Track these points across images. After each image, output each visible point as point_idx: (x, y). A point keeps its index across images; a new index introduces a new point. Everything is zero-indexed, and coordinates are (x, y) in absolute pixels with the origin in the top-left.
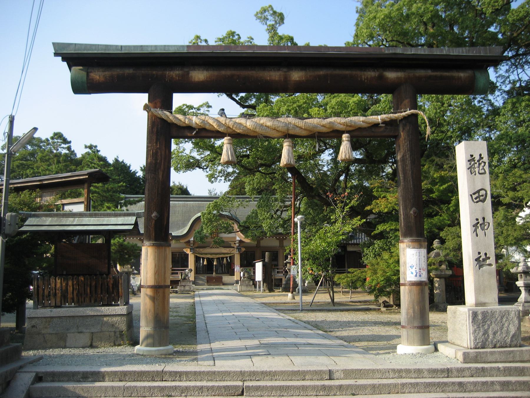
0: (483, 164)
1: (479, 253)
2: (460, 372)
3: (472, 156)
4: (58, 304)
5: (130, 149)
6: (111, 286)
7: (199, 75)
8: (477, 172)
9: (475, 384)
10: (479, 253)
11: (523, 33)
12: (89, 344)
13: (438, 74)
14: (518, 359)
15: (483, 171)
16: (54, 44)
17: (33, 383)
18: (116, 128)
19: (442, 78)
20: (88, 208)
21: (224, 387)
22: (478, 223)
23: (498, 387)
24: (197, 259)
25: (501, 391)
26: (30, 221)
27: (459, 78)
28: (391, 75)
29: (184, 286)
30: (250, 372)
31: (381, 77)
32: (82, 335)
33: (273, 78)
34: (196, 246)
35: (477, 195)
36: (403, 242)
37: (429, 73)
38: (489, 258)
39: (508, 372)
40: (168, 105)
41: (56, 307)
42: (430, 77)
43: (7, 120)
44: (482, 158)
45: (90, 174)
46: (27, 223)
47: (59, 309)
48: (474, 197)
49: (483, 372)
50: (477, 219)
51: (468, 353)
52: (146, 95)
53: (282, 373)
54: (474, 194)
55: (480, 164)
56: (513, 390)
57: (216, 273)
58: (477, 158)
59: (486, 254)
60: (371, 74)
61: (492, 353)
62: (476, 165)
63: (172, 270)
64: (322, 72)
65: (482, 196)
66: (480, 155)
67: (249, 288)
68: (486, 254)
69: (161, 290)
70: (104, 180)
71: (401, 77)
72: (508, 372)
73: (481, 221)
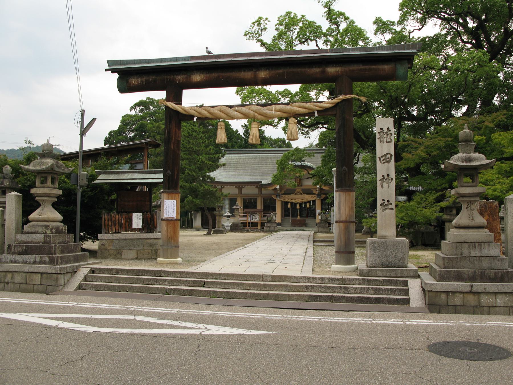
1: (383, 200)
3: (381, 129)
4: (117, 231)
6: (149, 220)
7: (197, 78)
11: (461, 21)
13: (367, 67)
14: (399, 275)
15: (389, 140)
16: (108, 61)
22: (384, 178)
23: (372, 292)
26: (101, 177)
28: (331, 70)
29: (270, 227)
31: (324, 72)
32: (131, 251)
34: (283, 192)
35: (384, 158)
37: (361, 67)
38: (391, 204)
40: (178, 100)
41: (116, 233)
42: (361, 70)
43: (80, 114)
44: (390, 131)
46: (99, 178)
47: (117, 234)
48: (382, 159)
49: (369, 282)
50: (383, 176)
52: (165, 92)
54: (382, 157)
55: (388, 135)
57: (300, 217)
58: (386, 130)
59: (388, 201)
60: (316, 70)
63: (264, 213)
64: (281, 71)
65: (388, 158)
66: (388, 128)
67: (325, 230)
68: (388, 201)
69: (307, 237)
71: (338, 71)
73: (386, 177)
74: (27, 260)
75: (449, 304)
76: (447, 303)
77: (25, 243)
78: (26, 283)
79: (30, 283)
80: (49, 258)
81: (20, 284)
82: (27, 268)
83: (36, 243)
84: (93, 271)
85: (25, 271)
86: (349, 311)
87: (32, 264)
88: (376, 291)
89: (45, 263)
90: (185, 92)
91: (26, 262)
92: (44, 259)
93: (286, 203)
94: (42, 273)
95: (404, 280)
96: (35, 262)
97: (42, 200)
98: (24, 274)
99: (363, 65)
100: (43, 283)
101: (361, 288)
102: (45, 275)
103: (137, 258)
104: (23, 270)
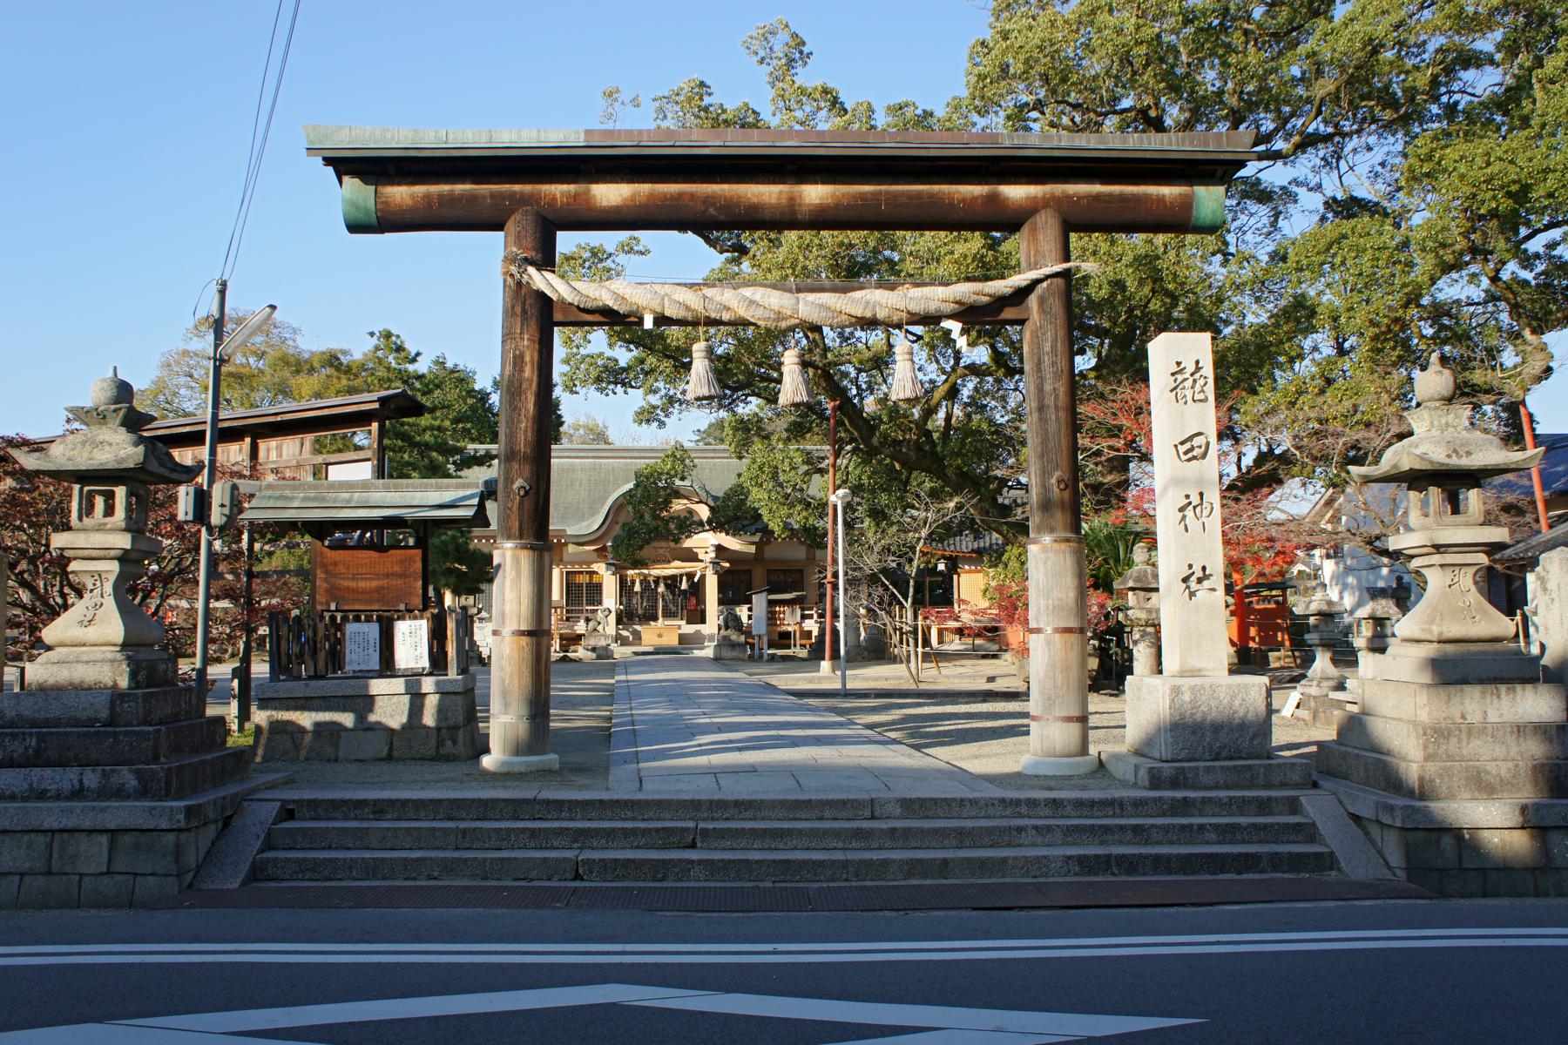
0: (1202, 381)
1: (1190, 566)
2: (1138, 804)
3: (1178, 364)
5: (478, 350)
8: (1189, 398)
9: (1166, 829)
10: (1190, 566)
12: (385, 753)
15: (1201, 396)
17: (275, 823)
18: (446, 303)
19: (1122, 198)
20: (380, 473)
21: (657, 830)
24: (625, 588)
25: (1219, 843)
27: (1160, 200)
30: (711, 801)
33: (766, 199)
35: (1188, 446)
36: (1035, 542)
39: (1242, 806)
43: (214, 289)
45: (382, 400)
47: (322, 682)
48: (1182, 449)
49: (1182, 807)
51: (1159, 769)
53: (773, 804)
54: (1182, 443)
56: (1244, 842)
58: (1191, 368)
59: (1204, 568)
61: (1208, 770)
62: (1189, 383)
66: (1197, 362)
68: (1204, 568)
70: (406, 415)
72: (1242, 806)
73: (1195, 500)
74: (45, 785)
75: (1466, 865)
76: (1460, 862)
77: (34, 723)
78: (49, 873)
79: (68, 869)
80: (139, 775)
81: (22, 875)
82: (53, 815)
83: (76, 723)
84: (288, 813)
85: (46, 826)
86: (1212, 904)
87: (68, 799)
88: (1227, 833)
89: (120, 793)
90: (560, 235)
91: (42, 795)
92: (115, 780)
93: (645, 576)
94: (113, 833)
95: (1288, 798)
96: (79, 793)
97: (92, 574)
98: (41, 840)
99: (1103, 183)
100: (118, 866)
101: (1183, 827)
102: (127, 839)
103: (389, 758)
104: (35, 823)
